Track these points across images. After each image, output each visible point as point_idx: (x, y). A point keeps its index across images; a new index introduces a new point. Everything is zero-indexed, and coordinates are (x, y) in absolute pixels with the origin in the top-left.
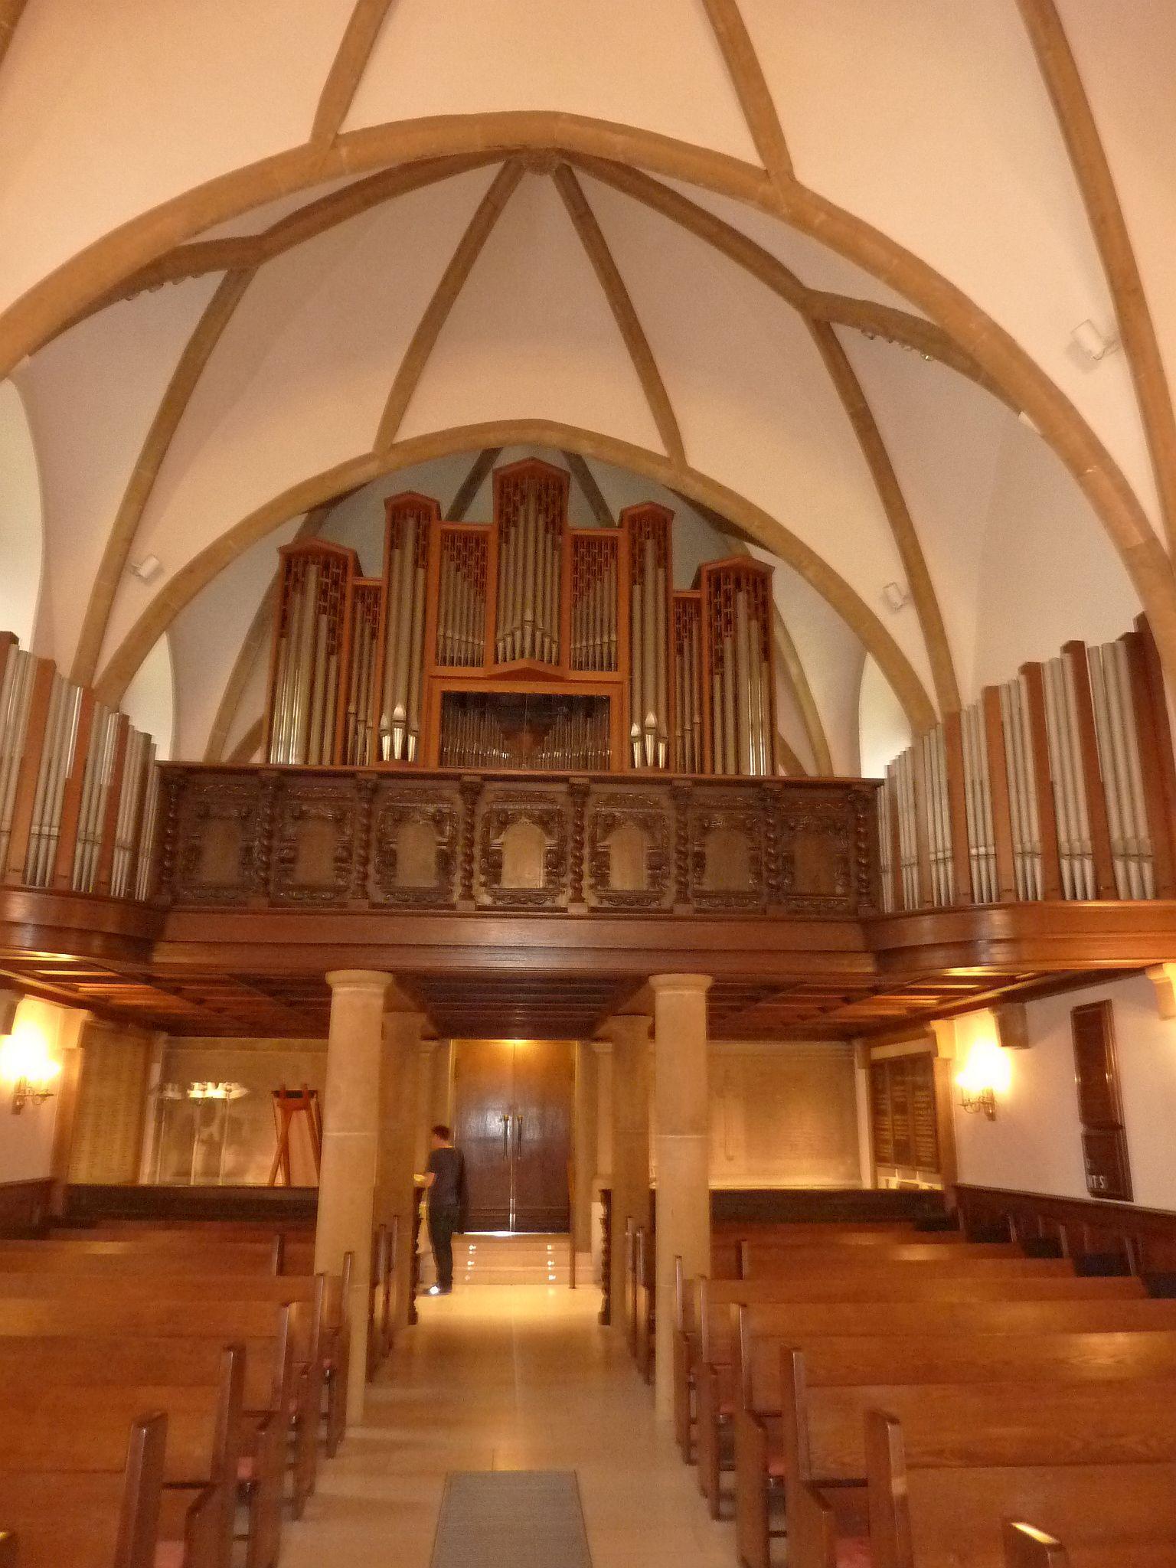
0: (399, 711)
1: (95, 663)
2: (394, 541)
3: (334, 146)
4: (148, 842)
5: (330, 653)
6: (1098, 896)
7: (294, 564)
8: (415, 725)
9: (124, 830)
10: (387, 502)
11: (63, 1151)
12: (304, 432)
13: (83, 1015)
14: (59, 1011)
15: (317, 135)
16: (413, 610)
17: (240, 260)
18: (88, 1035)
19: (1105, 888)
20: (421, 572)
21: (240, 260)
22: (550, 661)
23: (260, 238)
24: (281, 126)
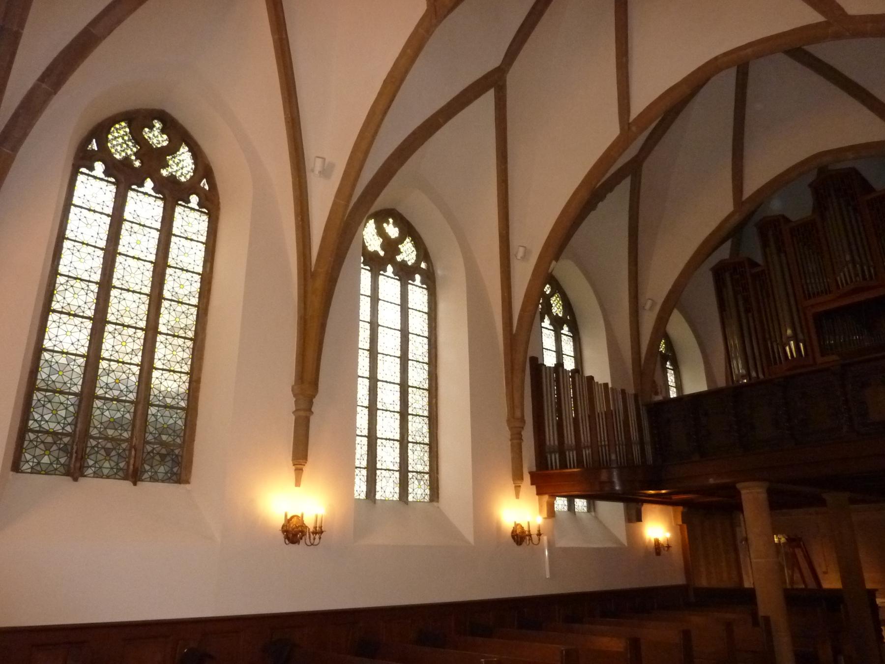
0: (789, 332)
1: (640, 357)
2: (765, 245)
3: (629, 128)
4: (647, 438)
5: (747, 311)
6: (561, 468)
7: (718, 272)
8: (801, 336)
9: (634, 435)
10: (810, 185)
11: (689, 569)
12: (696, 213)
13: (680, 509)
14: (670, 508)
15: (622, 129)
16: (783, 276)
17: (634, 168)
18: (686, 519)
19: (564, 465)
20: (783, 255)
21: (634, 168)
22: (871, 276)
23: (637, 156)
24: (609, 131)
